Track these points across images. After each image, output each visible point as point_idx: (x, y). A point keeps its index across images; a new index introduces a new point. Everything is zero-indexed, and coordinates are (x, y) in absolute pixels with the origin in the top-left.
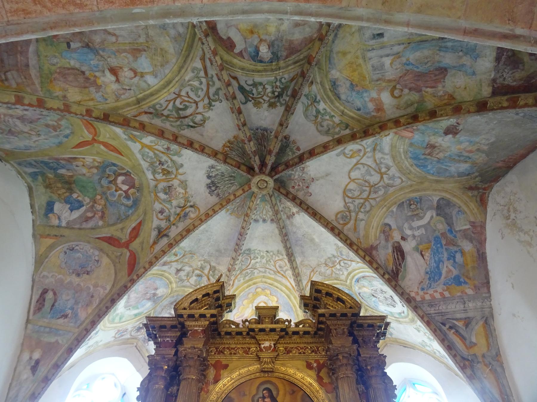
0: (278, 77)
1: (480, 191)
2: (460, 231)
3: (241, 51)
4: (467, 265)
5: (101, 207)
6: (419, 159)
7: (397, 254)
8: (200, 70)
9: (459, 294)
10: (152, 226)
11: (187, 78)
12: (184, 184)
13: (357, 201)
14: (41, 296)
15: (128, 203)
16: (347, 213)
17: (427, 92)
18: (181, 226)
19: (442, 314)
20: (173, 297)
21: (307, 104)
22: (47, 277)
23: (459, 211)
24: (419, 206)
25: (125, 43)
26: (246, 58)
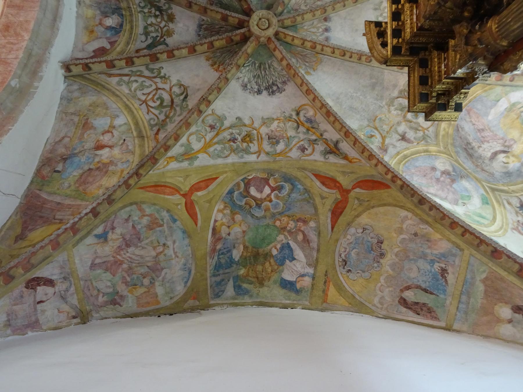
0: (139, 9)
3: (109, 43)
5: (291, 222)
8: (122, 79)
10: (322, 162)
11: (127, 91)
12: (266, 121)
14: (410, 308)
15: (287, 188)
18: (324, 125)
20: (457, 153)
22: (382, 298)
25: (75, 132)
26: (117, 39)
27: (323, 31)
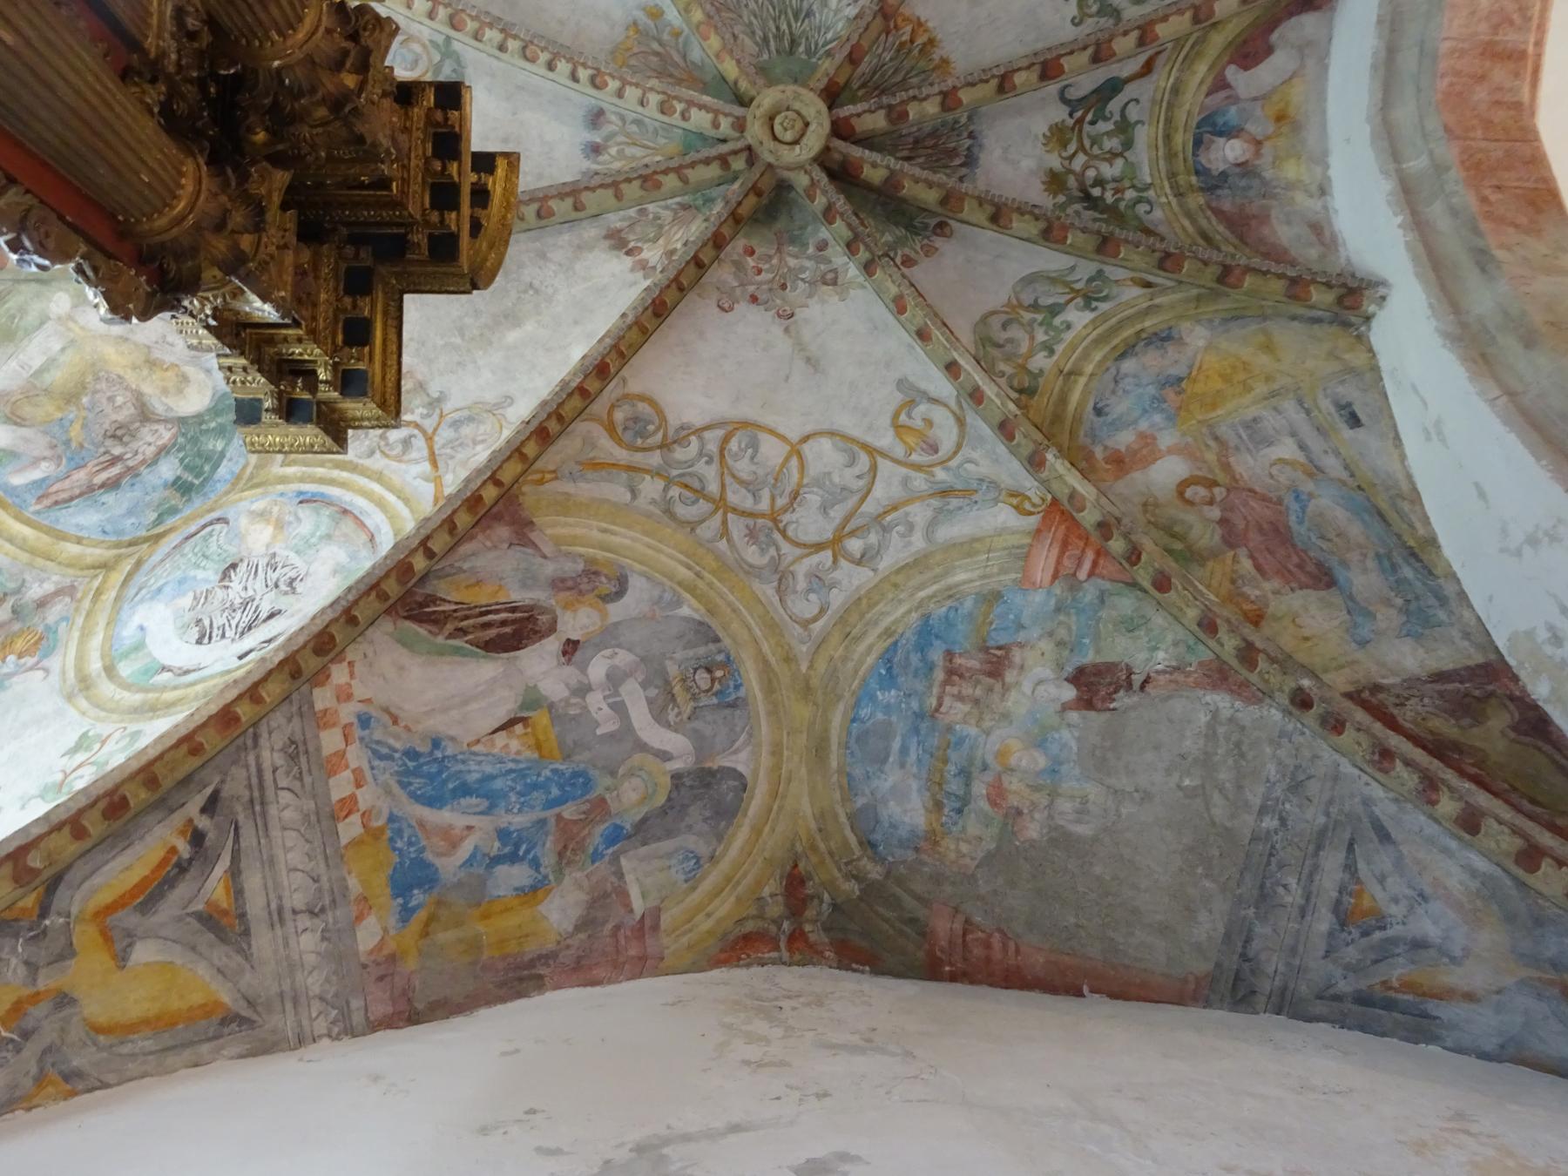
0: (1151, 193)
1: (786, 925)
2: (620, 875)
4: (486, 916)
6: (922, 647)
7: (504, 623)
9: (354, 884)
13: (710, 473)
16: (660, 435)
17: (1235, 560)
19: (258, 803)
21: (1069, 278)
23: (698, 859)
24: (705, 700)
26: (1208, 100)
27: (606, 148)
